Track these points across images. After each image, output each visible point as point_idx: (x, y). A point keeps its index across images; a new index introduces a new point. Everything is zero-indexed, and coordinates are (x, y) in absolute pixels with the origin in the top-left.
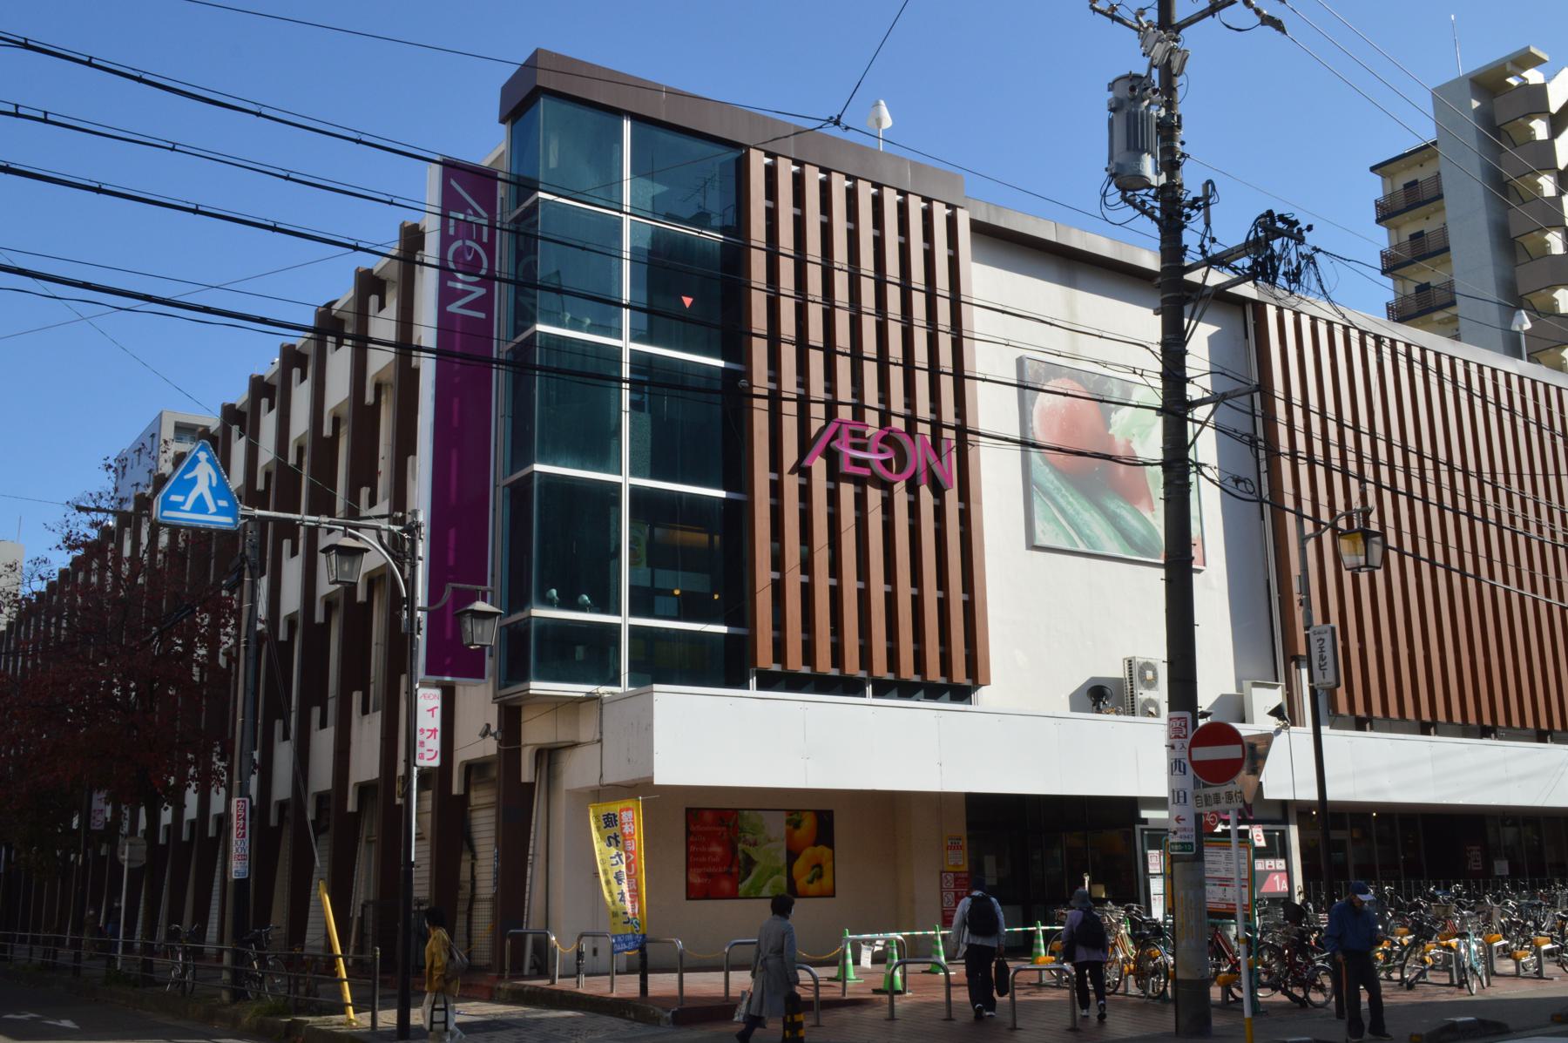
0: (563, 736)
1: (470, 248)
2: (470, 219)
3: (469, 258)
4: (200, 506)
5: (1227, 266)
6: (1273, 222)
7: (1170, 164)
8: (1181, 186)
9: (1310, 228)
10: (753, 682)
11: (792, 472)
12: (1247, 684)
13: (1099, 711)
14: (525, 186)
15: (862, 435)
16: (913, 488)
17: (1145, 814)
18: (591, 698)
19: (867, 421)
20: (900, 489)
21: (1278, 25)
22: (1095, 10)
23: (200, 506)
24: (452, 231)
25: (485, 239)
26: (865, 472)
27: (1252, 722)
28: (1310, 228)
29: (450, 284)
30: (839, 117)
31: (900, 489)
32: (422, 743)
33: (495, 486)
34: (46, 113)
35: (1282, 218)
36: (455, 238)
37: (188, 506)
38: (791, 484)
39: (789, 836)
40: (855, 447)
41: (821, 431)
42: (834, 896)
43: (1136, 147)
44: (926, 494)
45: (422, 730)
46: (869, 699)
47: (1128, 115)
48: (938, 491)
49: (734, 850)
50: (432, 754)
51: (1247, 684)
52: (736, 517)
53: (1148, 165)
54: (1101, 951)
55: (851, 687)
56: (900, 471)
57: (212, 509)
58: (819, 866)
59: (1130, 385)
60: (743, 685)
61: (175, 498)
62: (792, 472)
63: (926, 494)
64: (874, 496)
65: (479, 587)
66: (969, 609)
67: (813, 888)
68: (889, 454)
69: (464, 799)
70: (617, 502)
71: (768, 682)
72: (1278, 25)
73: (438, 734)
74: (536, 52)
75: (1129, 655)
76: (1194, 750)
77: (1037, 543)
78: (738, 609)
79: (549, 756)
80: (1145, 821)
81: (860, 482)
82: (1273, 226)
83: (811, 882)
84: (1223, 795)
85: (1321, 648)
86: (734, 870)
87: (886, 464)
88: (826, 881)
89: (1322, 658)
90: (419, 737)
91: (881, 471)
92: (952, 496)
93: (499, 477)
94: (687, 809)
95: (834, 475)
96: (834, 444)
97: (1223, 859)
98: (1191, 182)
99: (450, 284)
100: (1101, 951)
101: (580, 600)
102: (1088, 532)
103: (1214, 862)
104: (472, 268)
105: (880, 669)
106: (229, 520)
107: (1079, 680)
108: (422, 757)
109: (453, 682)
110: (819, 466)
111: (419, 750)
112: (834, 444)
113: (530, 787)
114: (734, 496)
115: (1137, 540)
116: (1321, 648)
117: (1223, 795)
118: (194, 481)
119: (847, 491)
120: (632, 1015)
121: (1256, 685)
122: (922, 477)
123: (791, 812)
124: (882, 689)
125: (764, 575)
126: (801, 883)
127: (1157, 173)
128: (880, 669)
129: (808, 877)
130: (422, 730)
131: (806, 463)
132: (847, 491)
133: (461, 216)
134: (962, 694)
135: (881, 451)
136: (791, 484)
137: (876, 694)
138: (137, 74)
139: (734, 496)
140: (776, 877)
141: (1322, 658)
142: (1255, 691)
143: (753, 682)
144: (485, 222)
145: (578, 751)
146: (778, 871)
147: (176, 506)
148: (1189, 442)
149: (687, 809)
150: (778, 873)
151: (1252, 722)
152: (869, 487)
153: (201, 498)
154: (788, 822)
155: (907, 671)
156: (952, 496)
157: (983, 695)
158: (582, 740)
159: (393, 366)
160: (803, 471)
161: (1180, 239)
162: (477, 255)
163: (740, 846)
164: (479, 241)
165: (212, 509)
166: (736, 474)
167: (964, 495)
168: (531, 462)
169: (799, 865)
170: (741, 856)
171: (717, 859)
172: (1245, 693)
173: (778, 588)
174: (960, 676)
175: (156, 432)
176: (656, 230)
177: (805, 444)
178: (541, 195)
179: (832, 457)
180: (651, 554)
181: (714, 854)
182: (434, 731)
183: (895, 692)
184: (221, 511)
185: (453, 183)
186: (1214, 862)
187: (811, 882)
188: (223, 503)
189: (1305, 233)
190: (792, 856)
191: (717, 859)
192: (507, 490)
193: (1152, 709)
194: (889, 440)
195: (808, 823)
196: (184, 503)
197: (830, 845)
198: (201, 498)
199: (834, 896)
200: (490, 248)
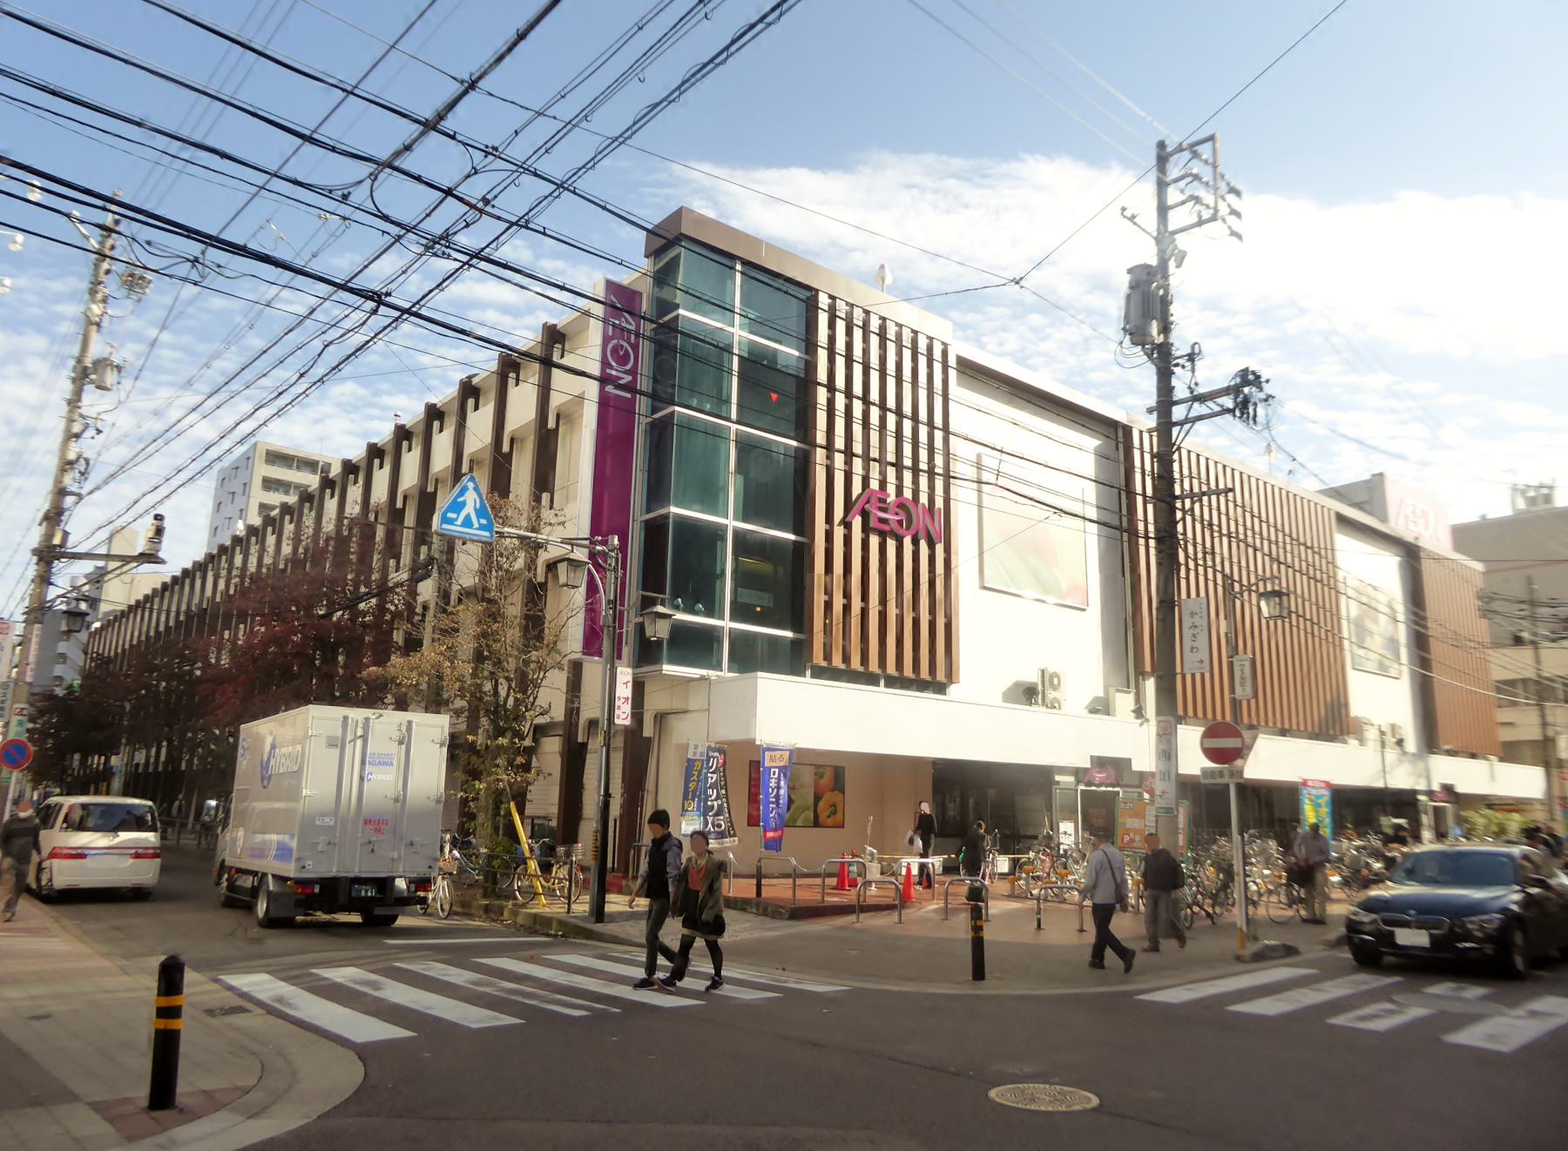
0: (677, 704)
1: (622, 346)
2: (624, 324)
3: (622, 353)
4: (467, 522)
7: (1166, 329)
8: (1172, 345)
9: (1267, 381)
10: (808, 673)
11: (839, 525)
12: (1112, 690)
13: (1031, 704)
14: (665, 306)
15: (884, 501)
16: (915, 542)
17: (1057, 778)
18: (703, 678)
19: (888, 491)
20: (907, 541)
21: (1239, 237)
22: (1125, 217)
23: (467, 522)
26: (887, 528)
27: (1115, 716)
28: (1267, 381)
29: (608, 371)
30: (1021, 279)
31: (907, 541)
32: (619, 707)
33: (633, 521)
34: (544, 228)
35: (1253, 373)
36: (613, 338)
37: (459, 522)
38: (839, 532)
39: (816, 783)
40: (881, 509)
41: (859, 496)
42: (843, 827)
43: (1147, 315)
44: (923, 545)
45: (619, 698)
46: (882, 688)
47: (1143, 293)
48: (931, 546)
50: (625, 716)
51: (1112, 690)
52: (801, 553)
53: (1154, 327)
55: (871, 679)
56: (908, 528)
57: (476, 525)
58: (834, 805)
60: (801, 673)
61: (450, 515)
62: (839, 525)
63: (923, 545)
64: (891, 545)
65: (661, 596)
66: (948, 627)
67: (830, 821)
68: (902, 517)
69: (584, 745)
70: (723, 539)
71: (819, 673)
72: (1239, 237)
73: (630, 701)
74: (681, 208)
75: (1043, 667)
77: (986, 585)
78: (798, 616)
79: (661, 718)
80: (1058, 783)
81: (883, 535)
82: (1249, 378)
83: (829, 817)
87: (900, 522)
88: (839, 816)
90: (617, 703)
91: (894, 526)
92: (940, 548)
93: (638, 515)
95: (866, 529)
96: (867, 506)
98: (1180, 346)
99: (608, 371)
101: (696, 608)
104: (623, 360)
105: (891, 669)
106: (487, 534)
107: (1008, 683)
108: (618, 718)
109: (581, 659)
110: (857, 523)
111: (617, 712)
112: (867, 506)
113: (649, 740)
114: (800, 539)
118: (464, 504)
119: (874, 541)
120: (754, 910)
121: (1118, 691)
122: (921, 534)
123: (818, 766)
124: (892, 682)
125: (819, 598)
126: (823, 817)
127: (1159, 334)
128: (891, 669)
129: (828, 813)
130: (619, 698)
131: (848, 519)
132: (874, 541)
133: (617, 322)
134: (940, 688)
135: (897, 514)
136: (839, 532)
137: (887, 686)
138: (603, 204)
139: (800, 539)
140: (806, 812)
142: (1118, 694)
143: (808, 673)
144: (633, 328)
145: (688, 716)
146: (806, 808)
147: (451, 521)
150: (808, 810)
151: (1115, 716)
152: (888, 539)
153: (468, 516)
154: (816, 774)
155: (908, 672)
156: (940, 548)
157: (952, 690)
158: (690, 709)
159: (533, 425)
160: (847, 525)
161: (1170, 382)
162: (626, 351)
164: (629, 343)
165: (476, 525)
166: (802, 523)
167: (947, 550)
168: (668, 504)
169: (821, 804)
172: (1110, 697)
173: (828, 606)
174: (941, 676)
175: (251, 455)
176: (752, 343)
177: (848, 504)
178: (681, 311)
179: (865, 515)
180: (743, 579)
182: (627, 699)
183: (915, 687)
184: (482, 527)
187: (829, 817)
188: (483, 521)
189: (1264, 385)
190: (817, 798)
192: (643, 525)
193: (1056, 705)
194: (901, 505)
195: (828, 774)
196: (456, 519)
197: (843, 792)
198: (468, 516)
199: (843, 827)
200: (635, 347)
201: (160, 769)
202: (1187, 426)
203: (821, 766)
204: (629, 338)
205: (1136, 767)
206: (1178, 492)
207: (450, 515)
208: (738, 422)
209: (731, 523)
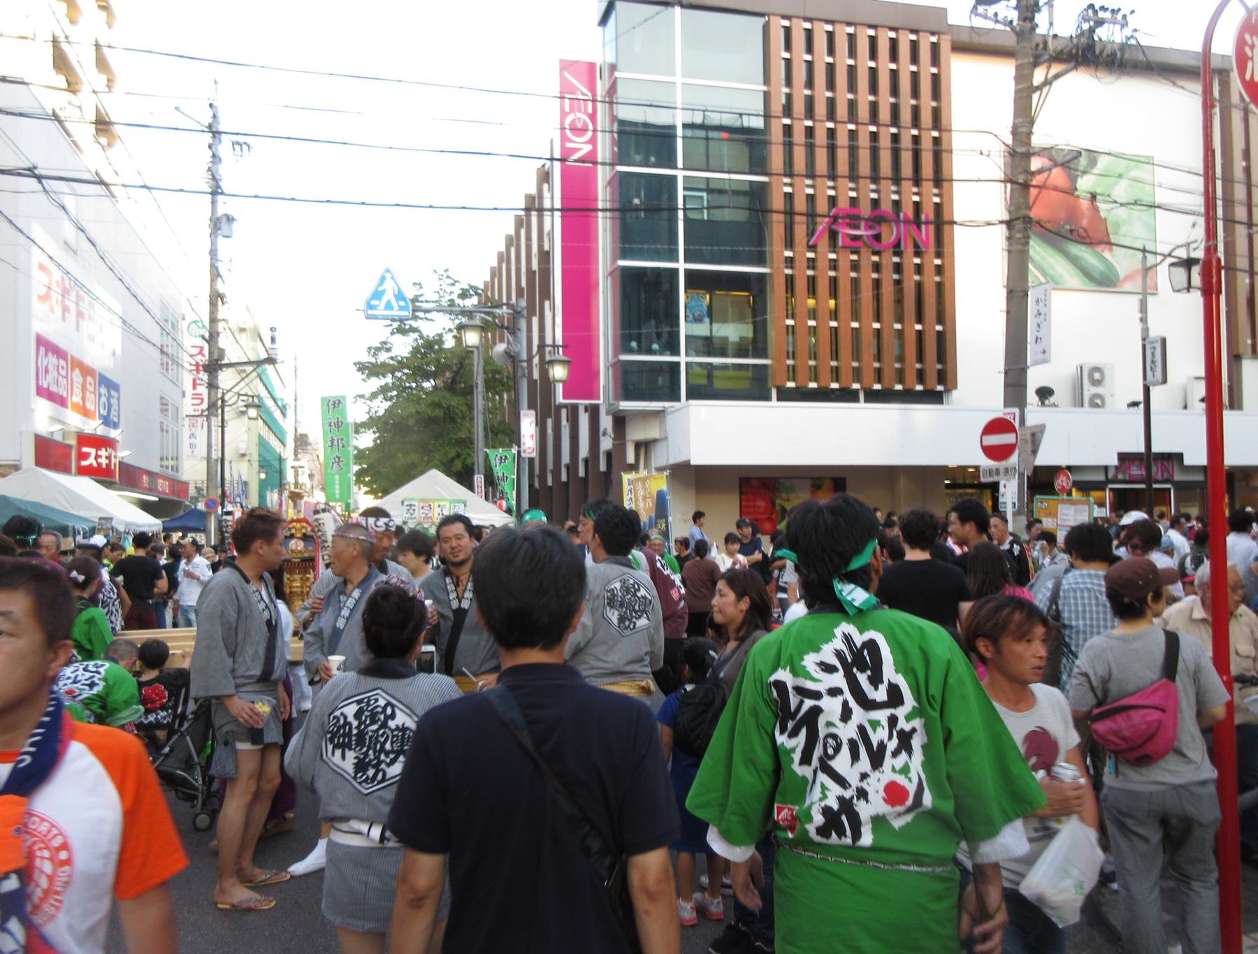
1: (580, 119)
5: (40, 182)
6: (1095, 12)
24: (567, 109)
25: (590, 111)
46: (862, 404)
49: (774, 504)
54: (423, 558)
59: (1096, 155)
61: (374, 302)
75: (1081, 362)
76: (984, 438)
84: (1002, 470)
85: (1153, 354)
86: (774, 516)
89: (1153, 362)
94: (741, 479)
97: (1072, 512)
100: (423, 558)
102: (1052, 272)
103: (1066, 515)
115: (1096, 275)
116: (1153, 354)
117: (1002, 470)
118: (384, 291)
123: (814, 479)
134: (934, 397)
137: (866, 401)
141: (1153, 362)
148: (1031, 203)
149: (741, 479)
163: (778, 501)
165: (396, 307)
170: (778, 508)
171: (762, 510)
181: (759, 507)
184: (401, 308)
185: (567, 75)
186: (1066, 515)
188: (402, 303)
191: (762, 510)
193: (1099, 402)
200: (593, 117)
201: (564, 478)
202: (1045, 90)
203: (818, 478)
204: (586, 108)
205: (1188, 461)
206: (558, 215)
207: (374, 302)
208: (684, 169)
209: (682, 266)
